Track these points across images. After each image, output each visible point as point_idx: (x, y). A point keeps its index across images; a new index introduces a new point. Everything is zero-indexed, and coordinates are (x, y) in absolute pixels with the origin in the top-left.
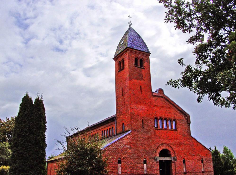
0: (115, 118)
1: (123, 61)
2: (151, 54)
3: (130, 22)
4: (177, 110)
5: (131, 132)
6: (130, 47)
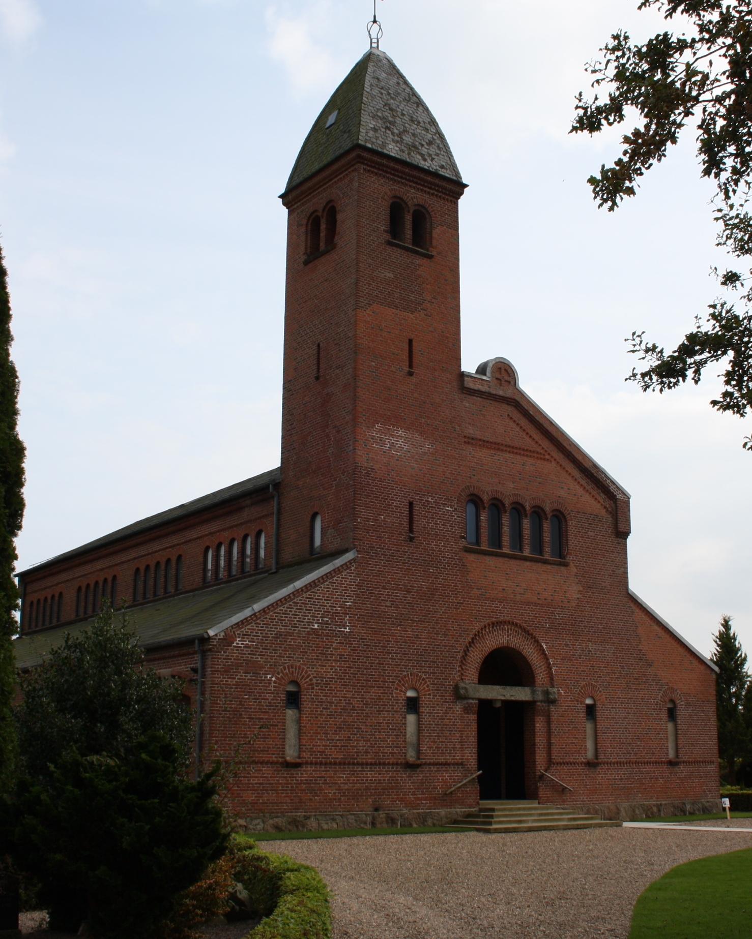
0: (277, 485)
1: (332, 212)
2: (466, 190)
3: (375, 21)
4: (570, 467)
5: (354, 560)
6: (370, 146)
